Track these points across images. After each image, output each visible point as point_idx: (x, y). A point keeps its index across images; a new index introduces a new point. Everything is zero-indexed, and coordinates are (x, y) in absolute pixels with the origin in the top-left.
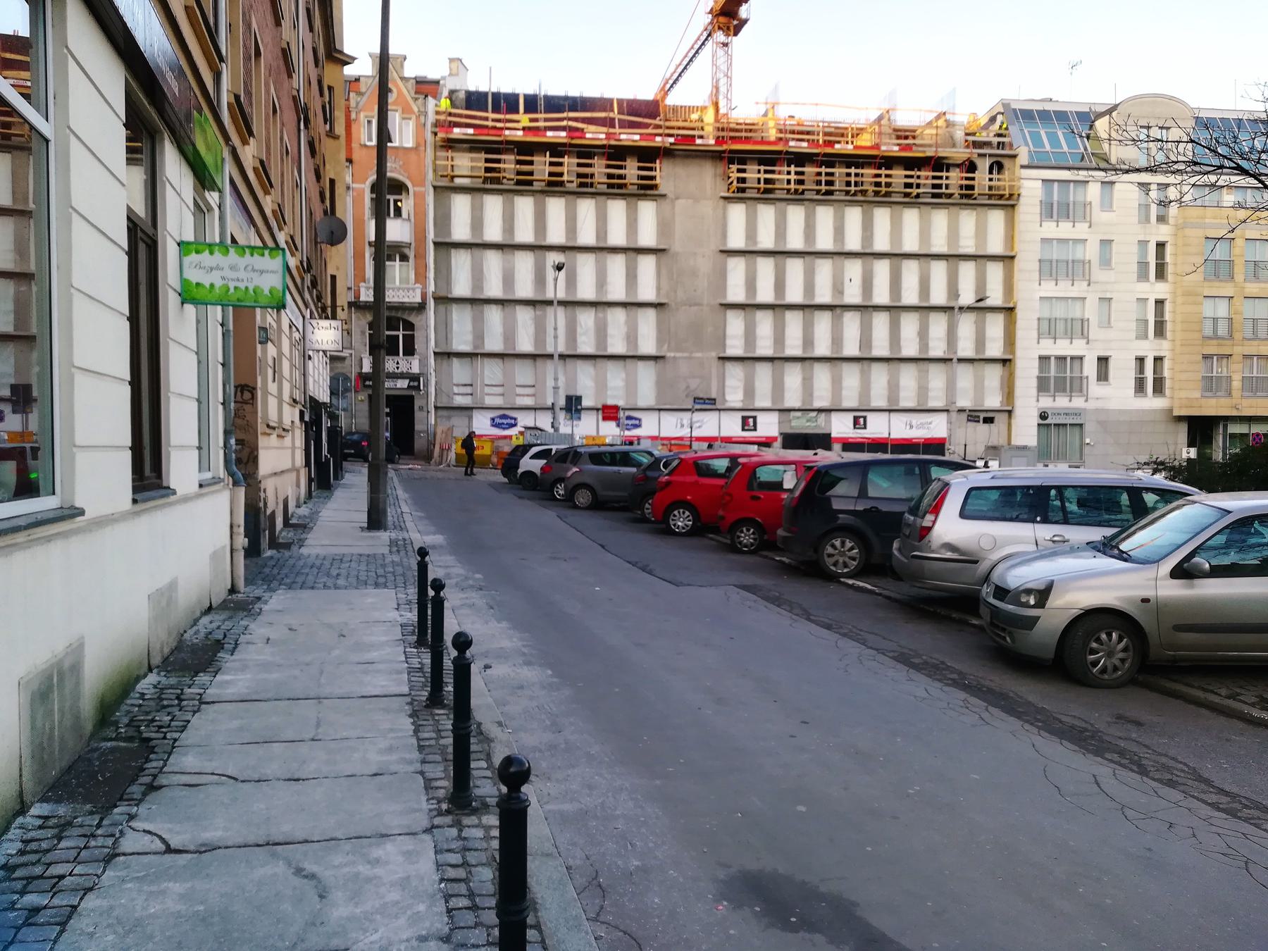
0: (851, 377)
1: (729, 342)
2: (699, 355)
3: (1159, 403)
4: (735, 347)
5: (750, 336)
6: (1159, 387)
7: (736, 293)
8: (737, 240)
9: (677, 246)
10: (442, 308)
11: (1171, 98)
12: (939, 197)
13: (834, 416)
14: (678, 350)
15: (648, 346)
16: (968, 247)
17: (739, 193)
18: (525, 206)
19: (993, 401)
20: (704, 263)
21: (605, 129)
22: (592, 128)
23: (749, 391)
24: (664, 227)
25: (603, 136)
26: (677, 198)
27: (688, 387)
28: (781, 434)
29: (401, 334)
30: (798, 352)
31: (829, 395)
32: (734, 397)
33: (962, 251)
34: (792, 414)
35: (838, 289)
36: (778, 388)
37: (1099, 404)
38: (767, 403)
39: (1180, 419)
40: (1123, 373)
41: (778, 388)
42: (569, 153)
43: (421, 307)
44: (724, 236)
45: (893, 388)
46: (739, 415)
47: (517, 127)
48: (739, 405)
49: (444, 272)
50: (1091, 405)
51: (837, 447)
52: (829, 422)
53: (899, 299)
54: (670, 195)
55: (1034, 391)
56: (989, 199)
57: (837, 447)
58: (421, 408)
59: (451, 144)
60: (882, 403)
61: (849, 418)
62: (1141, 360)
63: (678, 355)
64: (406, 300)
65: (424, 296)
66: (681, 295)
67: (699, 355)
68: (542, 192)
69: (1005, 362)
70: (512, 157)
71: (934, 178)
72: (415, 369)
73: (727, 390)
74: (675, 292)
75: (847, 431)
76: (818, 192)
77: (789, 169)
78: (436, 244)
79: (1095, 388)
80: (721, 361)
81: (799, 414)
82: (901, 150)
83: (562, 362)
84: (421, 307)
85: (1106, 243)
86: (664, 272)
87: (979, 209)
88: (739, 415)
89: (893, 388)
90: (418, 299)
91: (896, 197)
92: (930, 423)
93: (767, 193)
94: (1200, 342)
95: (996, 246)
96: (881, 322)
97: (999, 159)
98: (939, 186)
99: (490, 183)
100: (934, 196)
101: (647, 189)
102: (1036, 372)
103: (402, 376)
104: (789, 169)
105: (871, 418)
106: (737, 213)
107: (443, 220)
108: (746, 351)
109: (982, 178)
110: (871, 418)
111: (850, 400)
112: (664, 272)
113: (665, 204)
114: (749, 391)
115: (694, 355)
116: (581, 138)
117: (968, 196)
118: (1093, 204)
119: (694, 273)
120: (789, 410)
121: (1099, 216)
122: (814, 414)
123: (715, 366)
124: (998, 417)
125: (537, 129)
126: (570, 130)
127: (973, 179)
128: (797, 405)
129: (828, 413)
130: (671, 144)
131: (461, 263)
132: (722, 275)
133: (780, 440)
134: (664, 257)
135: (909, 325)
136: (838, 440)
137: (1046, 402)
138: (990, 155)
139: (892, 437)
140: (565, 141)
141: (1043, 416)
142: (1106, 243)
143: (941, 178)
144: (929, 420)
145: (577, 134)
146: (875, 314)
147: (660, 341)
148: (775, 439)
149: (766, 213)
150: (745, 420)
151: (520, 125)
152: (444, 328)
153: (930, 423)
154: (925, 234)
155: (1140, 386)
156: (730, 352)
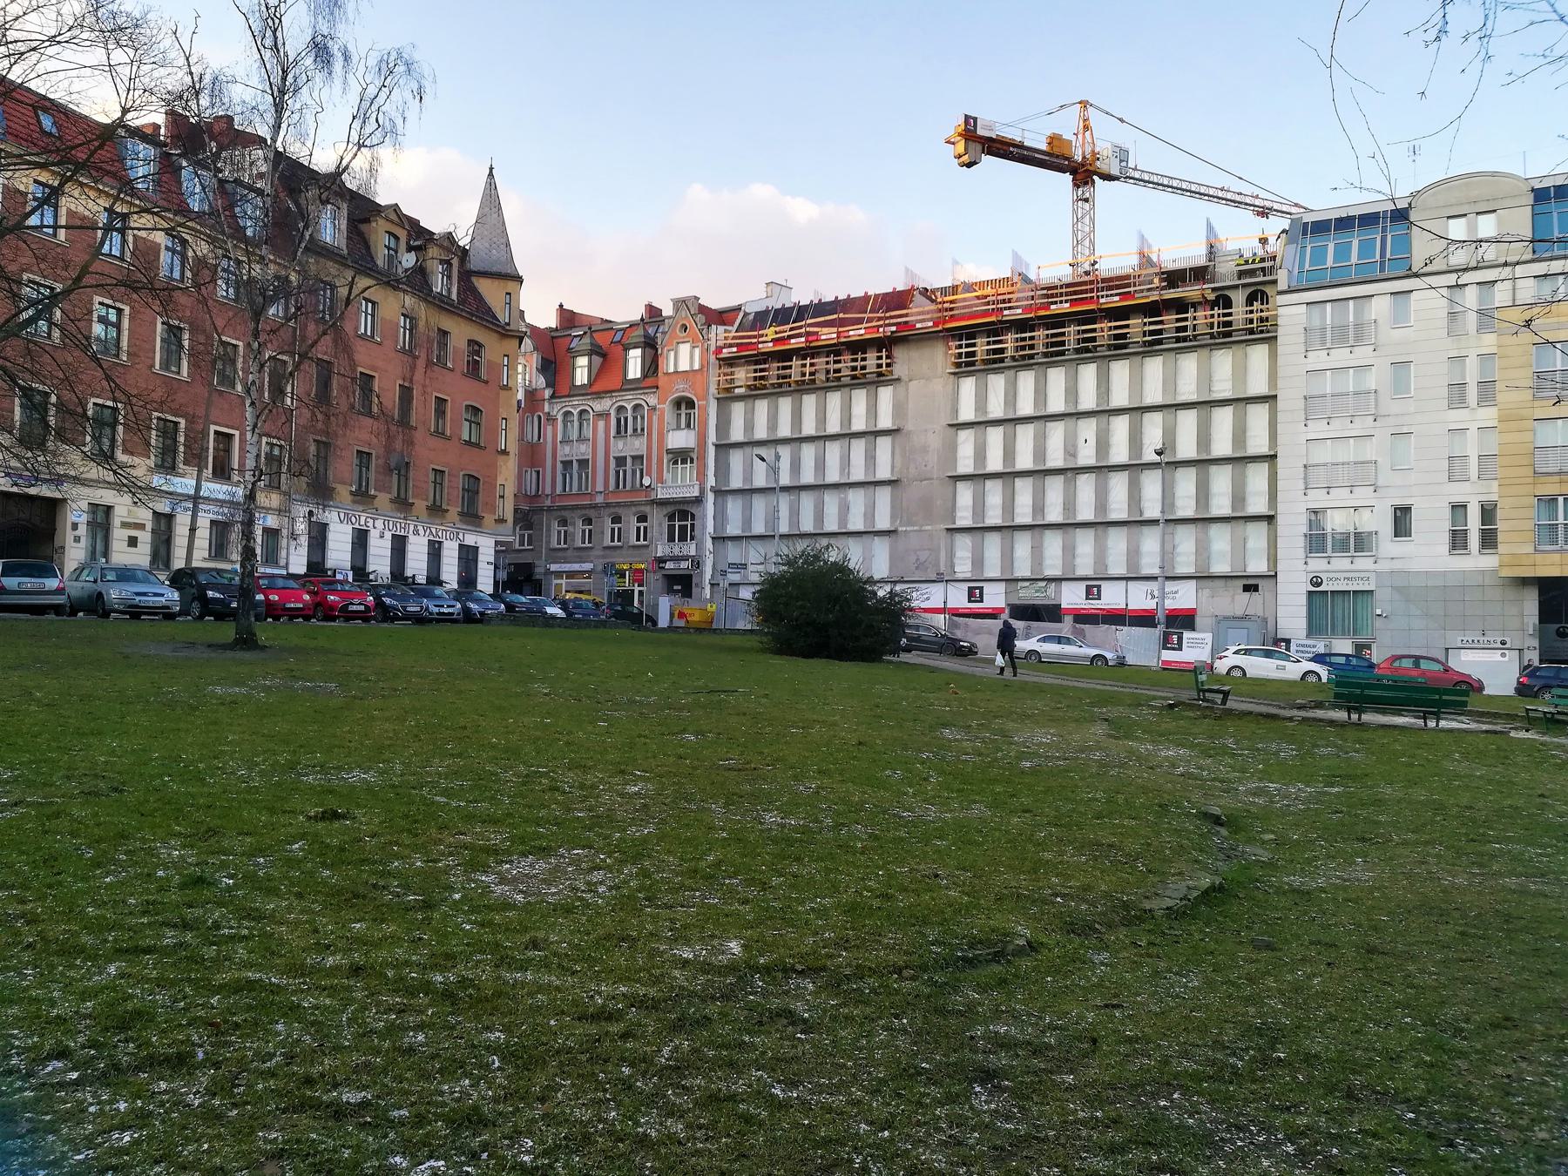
0: (1085, 544)
1: (959, 514)
2: (929, 528)
3: (1489, 561)
4: (964, 519)
5: (979, 506)
6: (1489, 540)
7: (965, 465)
8: (967, 413)
9: (909, 426)
10: (720, 500)
11: (1494, 174)
12: (1185, 342)
13: (1065, 586)
14: (910, 523)
15: (883, 523)
16: (1225, 391)
17: (965, 366)
18: (1088, 374)
19: (1257, 566)
20: (934, 441)
21: (835, 330)
22: (825, 330)
23: (978, 562)
24: (899, 409)
25: (835, 336)
26: (910, 380)
27: (918, 559)
28: (1009, 605)
29: (689, 523)
30: (1028, 520)
31: (1193, 558)
32: (963, 568)
33: (1182, 399)
34: (1021, 584)
35: (1071, 451)
36: (1008, 557)
37: (1397, 565)
38: (996, 574)
39: (1524, 582)
40: (1431, 526)
41: (1008, 557)
42: (1071, 322)
43: (699, 501)
44: (956, 411)
45: (1133, 554)
46: (965, 586)
47: (768, 338)
48: (968, 575)
49: (722, 470)
50: (1383, 566)
51: (1068, 619)
52: (1058, 593)
53: (1208, 451)
54: (904, 378)
55: (1301, 553)
56: (1176, 342)
57: (1068, 619)
58: (697, 585)
59: (730, 362)
60: (1120, 570)
61: (1082, 586)
62: (1459, 509)
63: (911, 528)
64: (675, 496)
65: (702, 491)
66: (912, 471)
67: (929, 528)
68: (873, 383)
69: (1270, 519)
70: (776, 365)
71: (1178, 320)
72: (693, 553)
73: (956, 561)
74: (908, 469)
75: (1079, 601)
76: (1212, 336)
77: (1212, 312)
78: (717, 446)
79: (1389, 546)
80: (949, 532)
81: (1027, 584)
82: (1121, 300)
83: (949, 535)
84: (699, 501)
85: (1401, 365)
86: (897, 451)
87: (1235, 347)
88: (965, 586)
89: (1133, 554)
90: (696, 494)
91: (1169, 343)
92: (1176, 592)
93: (995, 362)
94: (1530, 480)
95: (1258, 386)
96: (1118, 486)
97: (1259, 287)
98: (1185, 329)
99: (757, 390)
100: (1178, 340)
101: (882, 378)
102: (1446, 525)
103: (685, 558)
104: (1212, 312)
105: (989, 589)
106: (968, 385)
107: (724, 424)
108: (1234, 509)
109: (1239, 312)
110: (1105, 586)
111: (1085, 567)
112: (897, 451)
113: (901, 388)
114: (978, 562)
115: (923, 528)
116: (817, 340)
117: (1224, 336)
118: (1380, 322)
119: (925, 449)
120: (1017, 580)
121: (1391, 336)
122: (1043, 584)
123: (943, 539)
124: (1261, 583)
125: (783, 339)
126: (808, 334)
127: (1230, 314)
128: (1028, 574)
129: (1058, 583)
130: (892, 332)
131: (736, 459)
132: (951, 449)
133: (1007, 611)
134: (899, 438)
135: (1221, 480)
136: (1069, 611)
137: (1318, 564)
138: (1244, 286)
139: (1129, 608)
140: (804, 345)
141: (1316, 582)
142: (1401, 365)
143: (1186, 319)
144: (1174, 589)
145: (814, 338)
146: (1112, 474)
147: (893, 517)
148: (1002, 610)
149: (997, 383)
150: (1089, 590)
151: (769, 338)
152: (720, 516)
153: (1176, 592)
154: (1072, 392)
155: (1458, 540)
156: (960, 523)
